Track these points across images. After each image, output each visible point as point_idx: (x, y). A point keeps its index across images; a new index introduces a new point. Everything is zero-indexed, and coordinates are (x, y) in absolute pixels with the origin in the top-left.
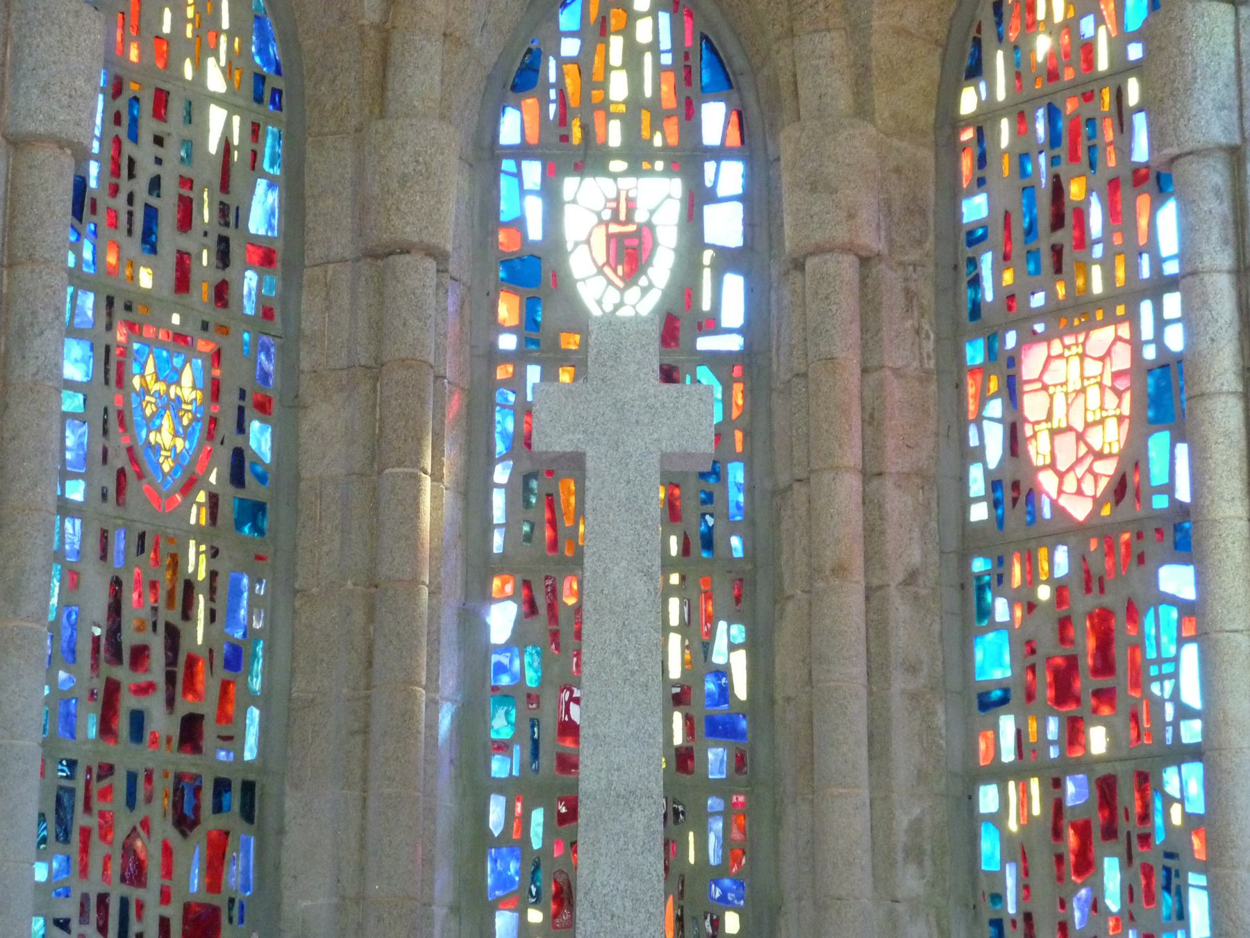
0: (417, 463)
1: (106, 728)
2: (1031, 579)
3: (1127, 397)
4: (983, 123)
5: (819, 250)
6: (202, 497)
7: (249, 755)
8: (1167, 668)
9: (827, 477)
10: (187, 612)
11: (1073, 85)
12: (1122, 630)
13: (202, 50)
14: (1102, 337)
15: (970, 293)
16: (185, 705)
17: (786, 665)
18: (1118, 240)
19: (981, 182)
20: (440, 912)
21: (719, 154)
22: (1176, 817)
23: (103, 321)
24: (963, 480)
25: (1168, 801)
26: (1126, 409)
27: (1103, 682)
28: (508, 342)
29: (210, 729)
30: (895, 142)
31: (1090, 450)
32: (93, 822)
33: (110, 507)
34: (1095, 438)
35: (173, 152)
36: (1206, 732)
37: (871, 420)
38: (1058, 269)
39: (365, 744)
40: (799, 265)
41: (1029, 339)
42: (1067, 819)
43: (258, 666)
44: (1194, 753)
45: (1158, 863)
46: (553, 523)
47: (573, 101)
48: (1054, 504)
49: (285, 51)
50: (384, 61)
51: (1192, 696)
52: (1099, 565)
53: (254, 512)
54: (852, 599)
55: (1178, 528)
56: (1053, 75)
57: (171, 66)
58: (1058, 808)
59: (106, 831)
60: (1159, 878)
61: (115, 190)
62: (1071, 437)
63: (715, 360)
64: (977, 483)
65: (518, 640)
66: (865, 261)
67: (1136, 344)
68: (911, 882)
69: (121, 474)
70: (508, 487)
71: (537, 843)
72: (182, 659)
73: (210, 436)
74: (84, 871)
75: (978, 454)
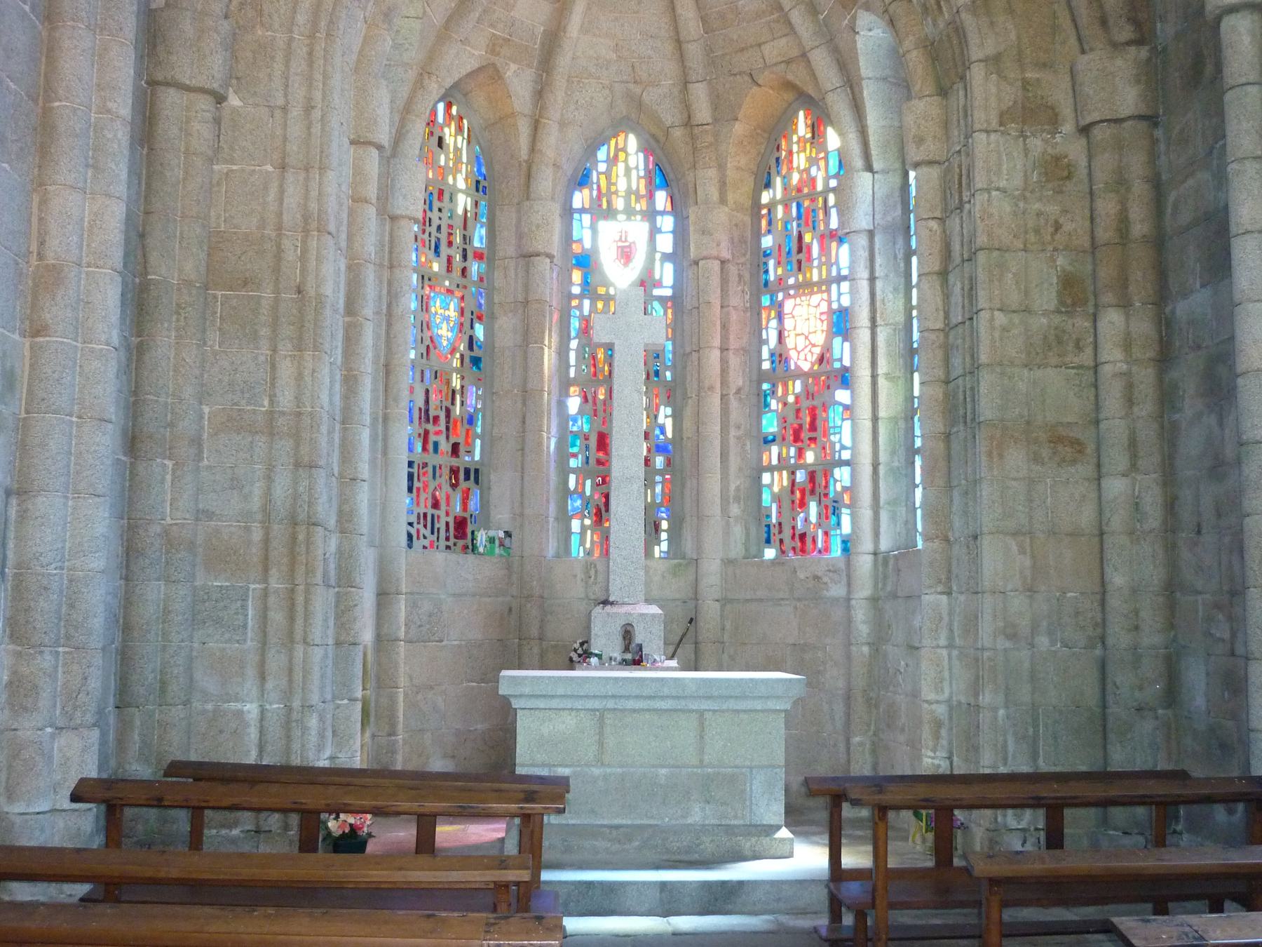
0: (542, 343)
1: (424, 449)
2: (786, 393)
3: (825, 322)
4: (771, 207)
5: (705, 258)
6: (458, 355)
7: (477, 457)
8: (837, 430)
9: (707, 351)
10: (453, 403)
11: (807, 195)
12: (821, 415)
13: (456, 170)
14: (816, 298)
15: (764, 276)
16: (453, 440)
17: (688, 424)
18: (824, 259)
19: (769, 232)
20: (551, 520)
21: (663, 213)
22: (839, 488)
23: (420, 285)
24: (760, 352)
25: (836, 481)
26: (825, 328)
27: (812, 435)
28: (576, 290)
29: (462, 449)
30: (735, 213)
31: (810, 343)
32: (420, 485)
33: (424, 361)
34: (813, 338)
35: (446, 214)
36: (852, 455)
37: (724, 327)
38: (800, 269)
39: (523, 455)
40: (696, 263)
41: (788, 296)
42: (797, 486)
43: (479, 423)
44: (847, 463)
45: (830, 504)
46: (595, 366)
47: (604, 190)
48: (796, 363)
49: (487, 170)
50: (529, 176)
51: (847, 442)
52: (812, 389)
53: (476, 361)
54: (715, 400)
55: (843, 376)
56: (799, 190)
57: (444, 178)
58: (793, 483)
59: (426, 486)
60: (830, 510)
61: (424, 232)
62: (803, 337)
63: (662, 300)
64: (765, 354)
65: (581, 412)
66: (723, 262)
67: (830, 303)
68: (735, 510)
69: (428, 347)
70: (577, 351)
71: (588, 493)
72: (452, 420)
73: (461, 331)
74: (418, 504)
75: (766, 342)
